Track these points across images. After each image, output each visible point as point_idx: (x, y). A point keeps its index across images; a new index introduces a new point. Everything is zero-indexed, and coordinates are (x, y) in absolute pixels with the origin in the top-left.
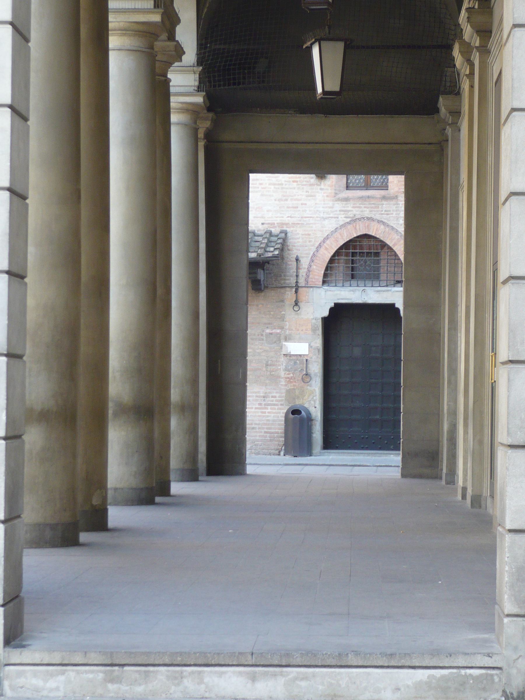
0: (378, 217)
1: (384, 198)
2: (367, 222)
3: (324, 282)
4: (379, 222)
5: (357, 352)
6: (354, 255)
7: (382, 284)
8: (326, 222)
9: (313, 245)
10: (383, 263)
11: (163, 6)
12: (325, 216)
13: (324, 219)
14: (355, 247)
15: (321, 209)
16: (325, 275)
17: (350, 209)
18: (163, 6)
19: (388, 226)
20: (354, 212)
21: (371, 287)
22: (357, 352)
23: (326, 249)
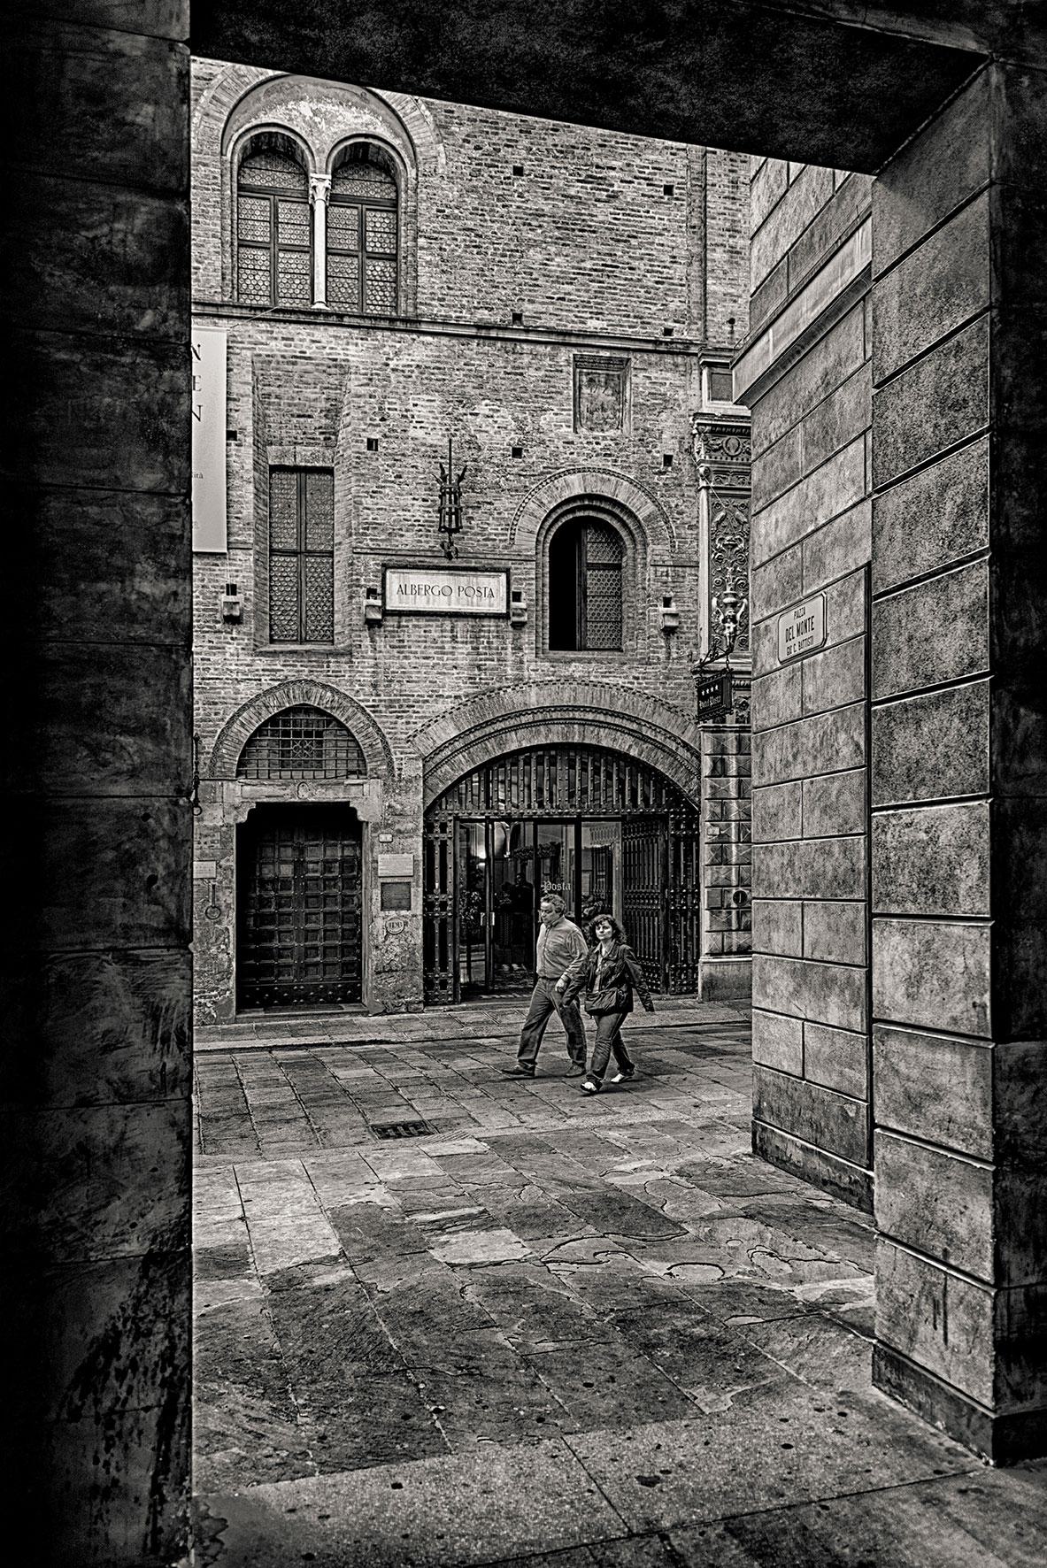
0: (322, 679)
1: (329, 654)
2: (306, 687)
3: (239, 774)
4: (324, 686)
5: (287, 870)
6: (286, 733)
7: (882, 799)
8: (242, 686)
9: (222, 720)
10: (327, 746)
11: (437, 926)
12: (240, 677)
13: (239, 682)
14: (286, 723)
15: (233, 667)
16: (241, 763)
17: (279, 667)
18: (437, 926)
19: (338, 692)
20: (286, 673)
21: (327, 248)
22: (287, 870)
23: (243, 725)
